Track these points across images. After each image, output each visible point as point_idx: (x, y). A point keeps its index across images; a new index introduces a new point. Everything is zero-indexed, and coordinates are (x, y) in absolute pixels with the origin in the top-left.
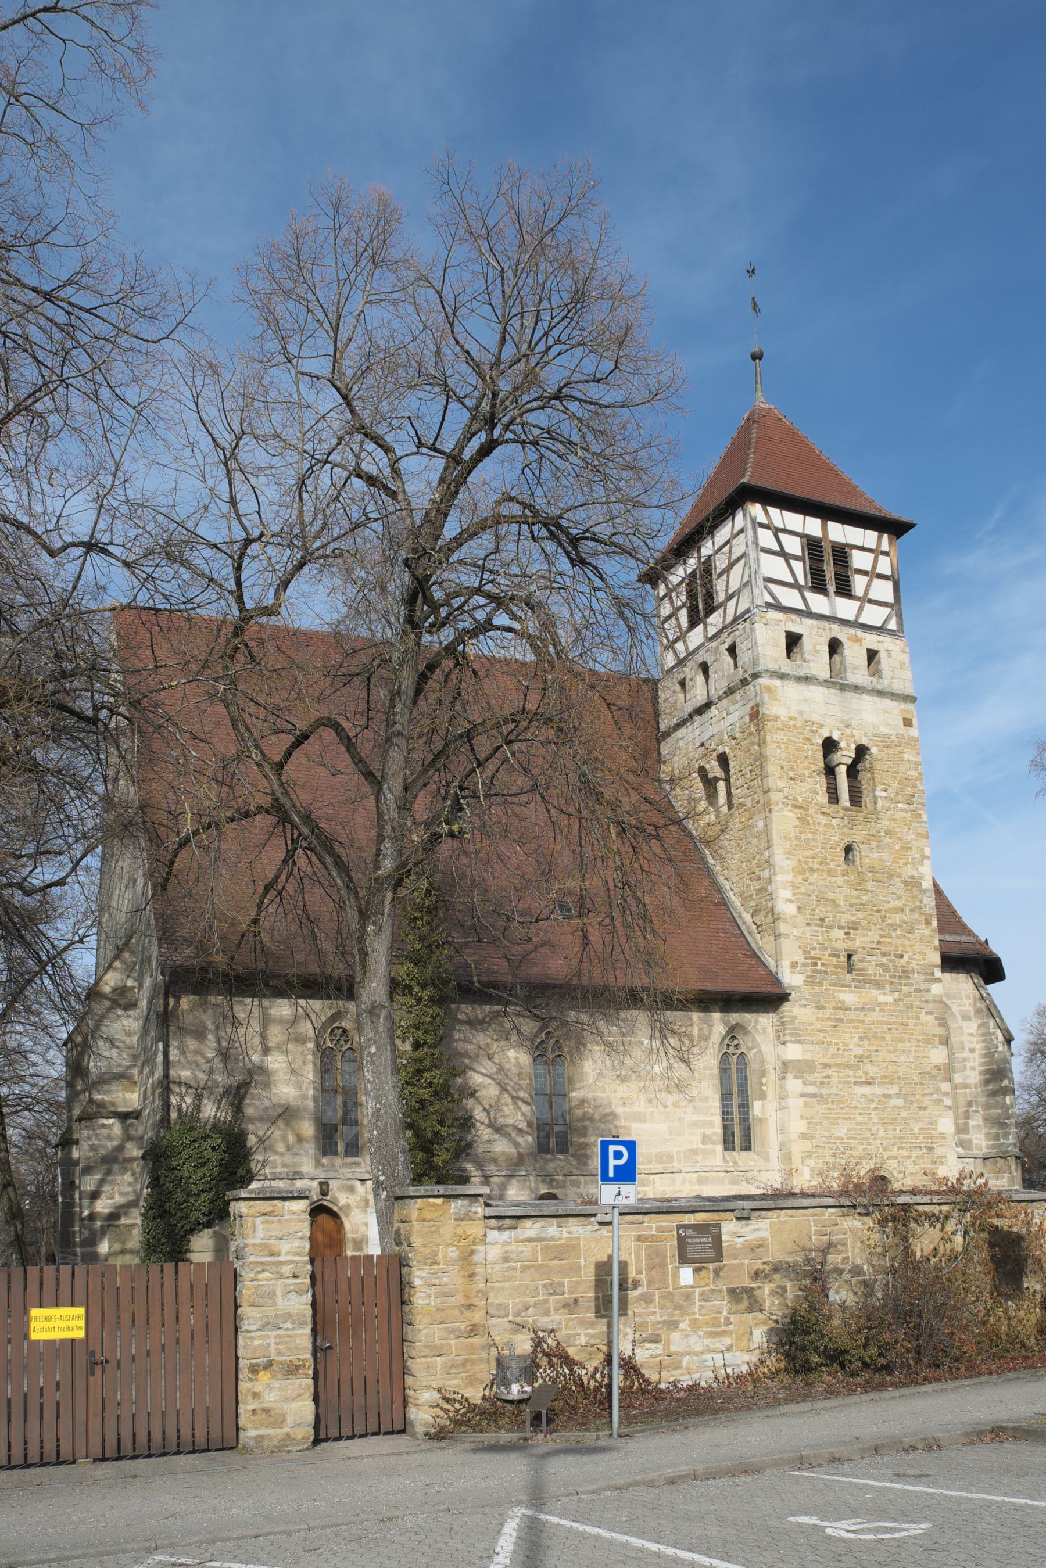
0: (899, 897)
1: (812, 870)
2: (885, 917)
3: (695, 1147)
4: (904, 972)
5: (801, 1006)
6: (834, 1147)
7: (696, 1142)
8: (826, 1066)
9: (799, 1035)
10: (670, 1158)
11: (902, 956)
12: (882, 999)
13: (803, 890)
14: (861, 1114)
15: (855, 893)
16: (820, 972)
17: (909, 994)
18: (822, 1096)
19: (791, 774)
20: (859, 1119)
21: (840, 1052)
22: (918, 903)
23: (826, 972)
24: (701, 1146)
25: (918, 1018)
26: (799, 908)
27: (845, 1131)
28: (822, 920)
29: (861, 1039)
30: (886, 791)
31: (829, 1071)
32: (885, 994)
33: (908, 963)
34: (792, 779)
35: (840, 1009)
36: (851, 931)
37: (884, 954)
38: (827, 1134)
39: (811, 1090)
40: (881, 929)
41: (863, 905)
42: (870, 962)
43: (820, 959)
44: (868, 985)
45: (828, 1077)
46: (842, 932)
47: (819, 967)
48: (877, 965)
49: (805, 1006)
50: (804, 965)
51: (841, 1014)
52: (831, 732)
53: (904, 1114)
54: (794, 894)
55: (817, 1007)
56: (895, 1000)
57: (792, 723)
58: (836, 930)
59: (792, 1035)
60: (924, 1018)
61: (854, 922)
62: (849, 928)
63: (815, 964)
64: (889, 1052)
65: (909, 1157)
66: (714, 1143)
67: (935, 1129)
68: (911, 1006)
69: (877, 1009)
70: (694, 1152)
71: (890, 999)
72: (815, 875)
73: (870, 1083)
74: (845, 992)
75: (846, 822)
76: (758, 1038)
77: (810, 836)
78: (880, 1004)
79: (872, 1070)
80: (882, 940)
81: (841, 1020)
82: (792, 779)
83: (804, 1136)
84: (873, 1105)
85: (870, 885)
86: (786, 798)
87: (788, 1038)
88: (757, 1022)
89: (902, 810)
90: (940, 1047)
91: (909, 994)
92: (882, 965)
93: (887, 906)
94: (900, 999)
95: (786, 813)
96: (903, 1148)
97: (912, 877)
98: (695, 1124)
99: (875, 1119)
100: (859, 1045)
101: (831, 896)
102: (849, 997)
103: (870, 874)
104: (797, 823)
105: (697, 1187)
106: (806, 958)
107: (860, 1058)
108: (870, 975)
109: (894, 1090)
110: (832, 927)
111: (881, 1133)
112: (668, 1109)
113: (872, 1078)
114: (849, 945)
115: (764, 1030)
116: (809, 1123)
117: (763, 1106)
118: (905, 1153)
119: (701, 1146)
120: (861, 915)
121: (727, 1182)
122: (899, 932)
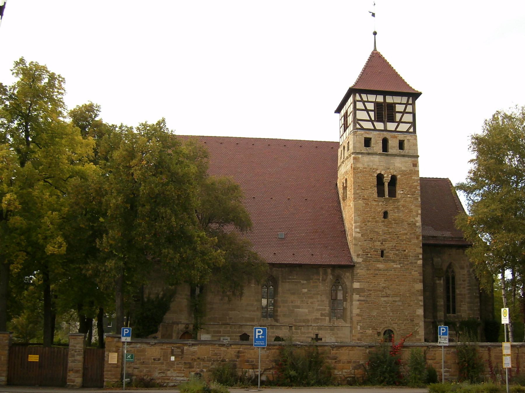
0: (405, 229)
1: (369, 221)
2: (399, 237)
3: (318, 317)
4: (405, 256)
5: (360, 269)
6: (371, 319)
7: (318, 315)
8: (369, 290)
9: (359, 279)
10: (308, 321)
11: (405, 251)
12: (395, 266)
13: (364, 228)
14: (382, 308)
15: (387, 229)
16: (369, 257)
17: (408, 264)
18: (367, 301)
19: (363, 188)
20: (382, 309)
21: (376, 285)
22: (414, 231)
23: (372, 257)
24: (320, 317)
25: (411, 273)
26: (362, 235)
27: (376, 313)
28: (372, 239)
29: (385, 281)
30: (403, 191)
31: (371, 292)
32: (396, 265)
33: (407, 253)
34: (363, 189)
35: (377, 270)
36: (384, 242)
37: (397, 250)
38: (368, 314)
39: (362, 298)
40: (397, 241)
41: (389, 233)
42: (391, 253)
43: (370, 253)
44: (389, 261)
45: (370, 294)
46: (380, 242)
47: (369, 256)
48: (394, 254)
49: (362, 269)
50: (362, 255)
51: (377, 272)
52: (381, 171)
53: (402, 308)
54: (360, 230)
55: (367, 270)
56: (401, 267)
57: (365, 169)
58: (377, 242)
59: (356, 279)
60: (413, 273)
61: (385, 239)
62: (383, 241)
63: (368, 255)
64: (397, 285)
65: (403, 323)
66: (326, 316)
67: (415, 313)
68: (408, 269)
69: (393, 270)
70: (318, 319)
71: (399, 266)
72: (370, 223)
73: (387, 297)
74: (380, 264)
75: (385, 203)
76: (345, 280)
77: (369, 209)
78: (395, 268)
79: (389, 292)
80: (397, 245)
81: (377, 274)
82: (363, 189)
83: (358, 315)
84: (389, 305)
85: (394, 226)
86: (360, 196)
87: (355, 281)
88: (345, 275)
89: (409, 197)
90: (419, 283)
91: (408, 264)
92: (396, 254)
93: (400, 233)
94: (403, 266)
95: (359, 202)
96: (400, 320)
97: (412, 222)
98: (318, 310)
99: (389, 309)
100: (384, 283)
101: (376, 230)
102: (381, 266)
103: (393, 222)
104: (364, 205)
105: (317, 331)
106: (363, 253)
107: (384, 288)
108: (391, 258)
109: (398, 299)
110: (376, 241)
111: (391, 314)
112: (308, 304)
113: (389, 295)
114: (382, 247)
115: (348, 278)
116: (361, 310)
117: (346, 304)
118: (401, 322)
119: (320, 317)
120: (388, 236)
121: (329, 330)
122: (404, 242)
